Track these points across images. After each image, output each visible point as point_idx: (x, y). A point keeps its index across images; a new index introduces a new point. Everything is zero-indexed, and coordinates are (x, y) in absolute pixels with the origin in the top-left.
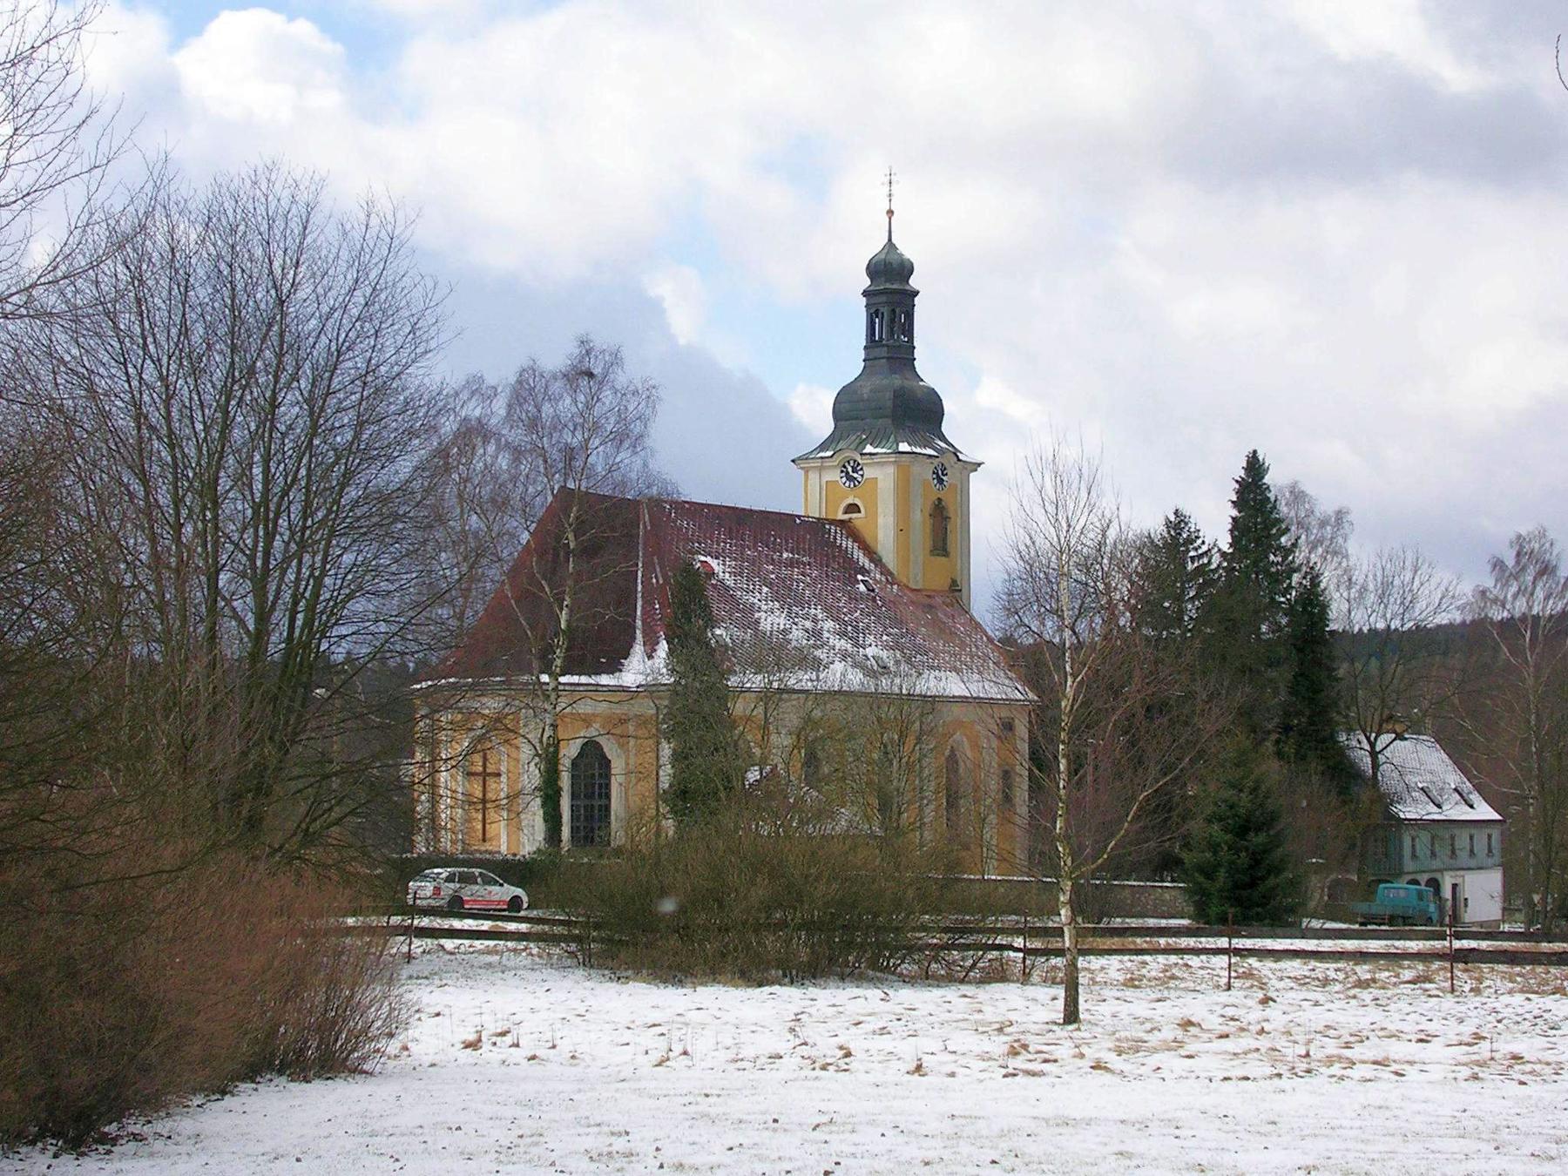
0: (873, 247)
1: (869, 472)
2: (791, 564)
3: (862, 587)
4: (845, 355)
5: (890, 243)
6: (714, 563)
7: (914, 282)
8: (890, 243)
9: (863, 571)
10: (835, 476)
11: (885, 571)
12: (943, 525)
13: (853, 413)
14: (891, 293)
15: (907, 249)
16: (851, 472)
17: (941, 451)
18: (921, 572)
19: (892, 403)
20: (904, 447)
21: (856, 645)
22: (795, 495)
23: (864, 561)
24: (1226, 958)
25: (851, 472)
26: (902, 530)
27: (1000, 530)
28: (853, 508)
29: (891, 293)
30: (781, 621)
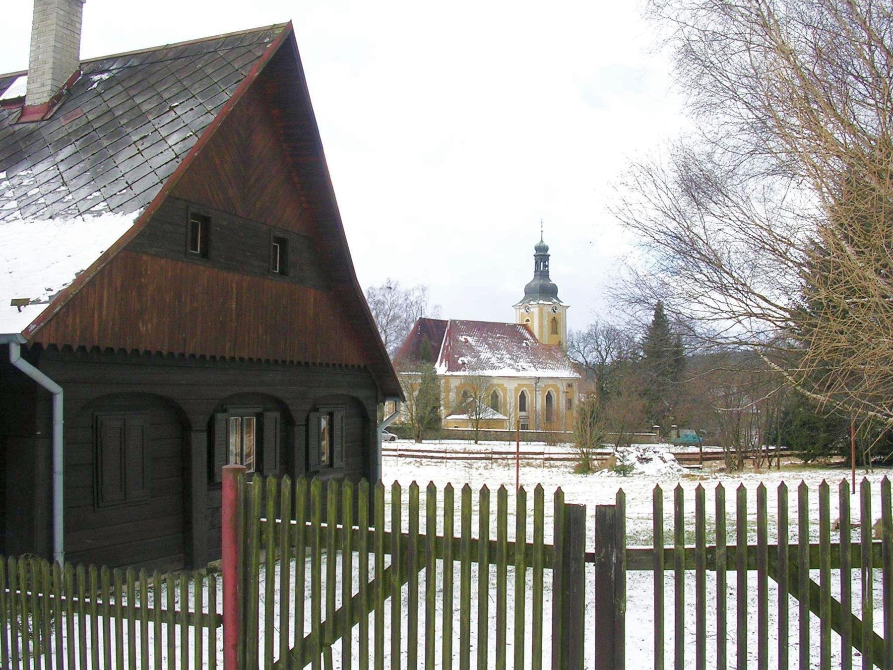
0: (537, 242)
1: (532, 310)
2: (499, 338)
3: (524, 345)
4: (528, 275)
5: (542, 241)
6: (469, 339)
7: (549, 252)
8: (542, 241)
9: (527, 339)
10: (523, 311)
11: (535, 339)
12: (555, 325)
13: (531, 293)
14: (542, 255)
15: (546, 243)
16: (527, 309)
17: (554, 303)
18: (554, 340)
19: (543, 289)
20: (541, 302)
21: (516, 362)
22: (511, 317)
23: (528, 336)
24: (520, 450)
25: (527, 309)
26: (541, 327)
27: (576, 324)
28: (528, 320)
29: (542, 255)
30: (489, 355)
